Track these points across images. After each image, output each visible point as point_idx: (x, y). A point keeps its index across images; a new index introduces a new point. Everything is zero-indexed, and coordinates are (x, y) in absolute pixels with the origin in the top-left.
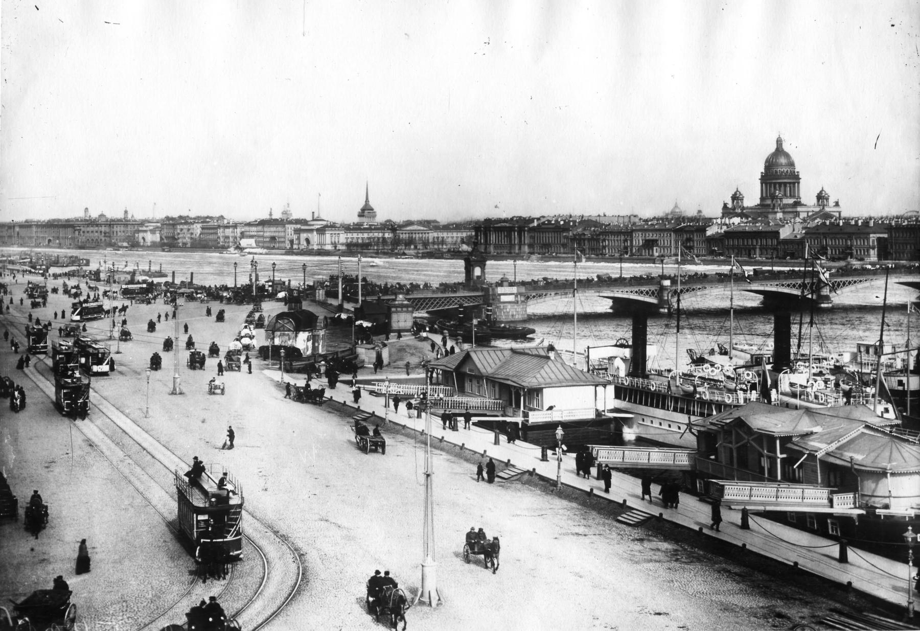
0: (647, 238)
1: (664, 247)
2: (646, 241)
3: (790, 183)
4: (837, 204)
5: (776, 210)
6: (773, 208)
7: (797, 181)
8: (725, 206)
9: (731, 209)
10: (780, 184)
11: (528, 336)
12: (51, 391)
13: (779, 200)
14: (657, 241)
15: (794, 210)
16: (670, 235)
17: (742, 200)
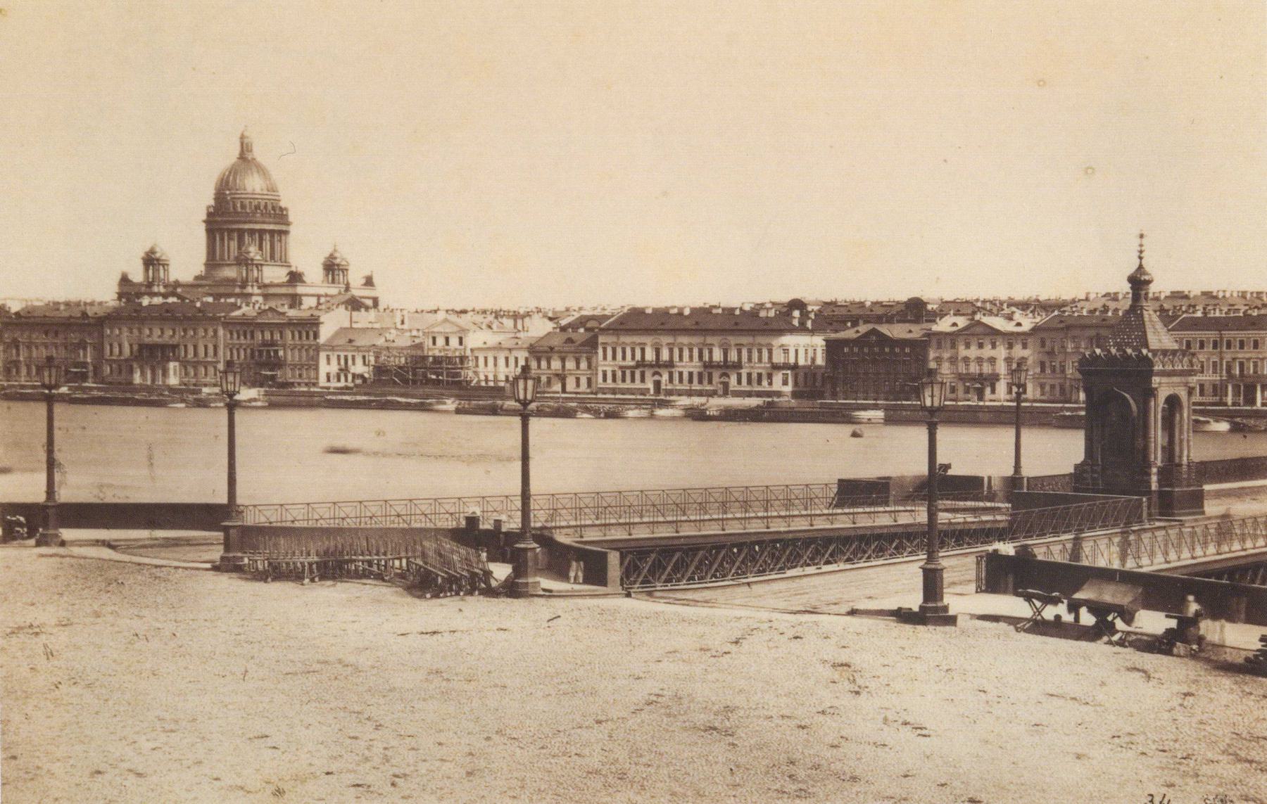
0: (147, 340)
1: (196, 365)
2: (142, 347)
3: (272, 232)
4: (369, 282)
5: (249, 290)
6: (243, 286)
7: (284, 228)
8: (125, 280)
9: (141, 285)
10: (252, 232)
11: (1034, 600)
12: (1254, 644)
13: (255, 269)
14: (174, 347)
15: (290, 291)
16: (215, 332)
17: (165, 265)
